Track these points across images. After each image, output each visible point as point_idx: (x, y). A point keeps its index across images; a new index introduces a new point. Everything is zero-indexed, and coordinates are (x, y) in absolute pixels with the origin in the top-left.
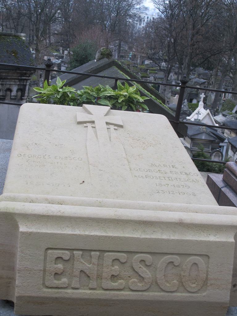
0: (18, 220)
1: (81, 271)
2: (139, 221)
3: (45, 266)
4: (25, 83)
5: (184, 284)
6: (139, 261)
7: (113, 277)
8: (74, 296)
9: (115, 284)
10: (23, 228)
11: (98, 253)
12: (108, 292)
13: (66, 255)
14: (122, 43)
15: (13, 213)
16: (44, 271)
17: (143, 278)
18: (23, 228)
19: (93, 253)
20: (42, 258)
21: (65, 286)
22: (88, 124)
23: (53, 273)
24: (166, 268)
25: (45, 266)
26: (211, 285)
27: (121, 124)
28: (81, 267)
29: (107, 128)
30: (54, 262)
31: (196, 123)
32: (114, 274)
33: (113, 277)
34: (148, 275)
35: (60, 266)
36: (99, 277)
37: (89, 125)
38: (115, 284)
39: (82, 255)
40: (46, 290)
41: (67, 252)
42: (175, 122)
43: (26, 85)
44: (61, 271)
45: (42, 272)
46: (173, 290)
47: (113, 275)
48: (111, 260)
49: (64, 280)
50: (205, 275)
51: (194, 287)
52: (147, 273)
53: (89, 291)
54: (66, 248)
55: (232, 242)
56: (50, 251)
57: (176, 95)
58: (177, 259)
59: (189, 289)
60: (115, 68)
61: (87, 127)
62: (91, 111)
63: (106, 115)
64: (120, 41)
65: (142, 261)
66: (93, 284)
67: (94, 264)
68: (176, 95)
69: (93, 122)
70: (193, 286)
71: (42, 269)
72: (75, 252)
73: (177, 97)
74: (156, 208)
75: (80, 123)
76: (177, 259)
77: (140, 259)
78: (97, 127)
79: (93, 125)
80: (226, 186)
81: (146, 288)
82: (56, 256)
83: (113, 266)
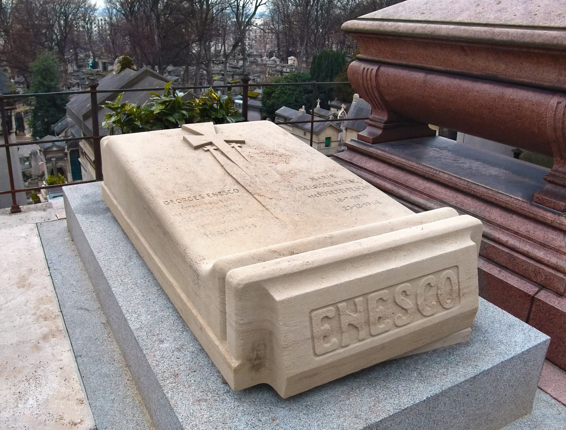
0: (267, 287)
2: (389, 249)
4: (9, 114)
5: (442, 302)
8: (347, 354)
10: (280, 295)
11: (361, 298)
13: (330, 311)
14: (78, 51)
15: (260, 281)
16: (313, 338)
17: (406, 310)
19: (357, 300)
23: (322, 337)
32: (381, 315)
35: (327, 326)
36: (368, 323)
40: (317, 359)
43: (11, 116)
45: (310, 341)
49: (334, 340)
50: (457, 287)
54: (330, 303)
58: (431, 279)
60: (150, 79)
64: (75, 49)
66: (363, 333)
71: (309, 336)
76: (431, 279)
77: (402, 290)
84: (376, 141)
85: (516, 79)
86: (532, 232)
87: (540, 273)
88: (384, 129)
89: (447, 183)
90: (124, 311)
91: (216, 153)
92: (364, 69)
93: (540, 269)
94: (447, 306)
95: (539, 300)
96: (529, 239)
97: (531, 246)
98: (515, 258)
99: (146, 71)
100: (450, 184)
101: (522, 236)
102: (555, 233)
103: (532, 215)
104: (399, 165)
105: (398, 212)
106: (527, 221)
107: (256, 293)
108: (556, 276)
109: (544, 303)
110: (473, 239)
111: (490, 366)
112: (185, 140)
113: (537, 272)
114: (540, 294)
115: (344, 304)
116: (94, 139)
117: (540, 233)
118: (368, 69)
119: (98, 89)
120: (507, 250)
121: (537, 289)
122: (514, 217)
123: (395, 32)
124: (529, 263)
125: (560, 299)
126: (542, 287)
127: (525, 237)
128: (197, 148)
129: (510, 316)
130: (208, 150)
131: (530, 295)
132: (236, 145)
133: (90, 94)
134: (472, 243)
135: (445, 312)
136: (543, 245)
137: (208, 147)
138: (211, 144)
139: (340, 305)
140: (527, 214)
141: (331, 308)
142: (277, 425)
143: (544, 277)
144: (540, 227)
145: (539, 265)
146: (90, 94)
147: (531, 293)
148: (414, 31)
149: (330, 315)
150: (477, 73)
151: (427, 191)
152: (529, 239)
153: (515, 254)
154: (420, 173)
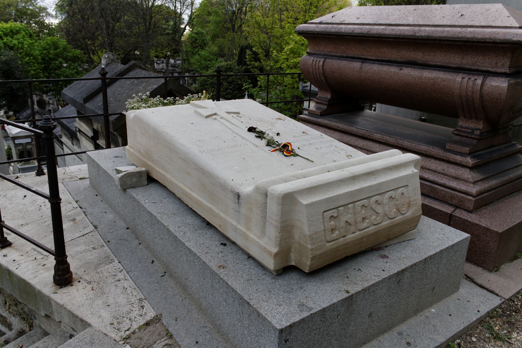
9: (365, 225)
13: (334, 213)
17: (378, 213)
18: (305, 201)
32: (364, 216)
38: (365, 225)
40: (327, 244)
47: (363, 218)
56: (325, 214)
84: (323, 114)
85: (430, 63)
86: (446, 170)
87: (454, 197)
88: (328, 105)
89: (380, 140)
90: (173, 231)
91: (221, 120)
92: (313, 60)
93: (454, 194)
94: (403, 213)
95: (456, 216)
96: (445, 175)
97: (446, 179)
98: (435, 189)
99: (134, 64)
100: (382, 141)
101: (439, 173)
102: (463, 169)
103: (445, 158)
104: (343, 130)
105: (361, 155)
106: (442, 163)
107: (289, 199)
108: (466, 199)
109: (459, 218)
110: (415, 168)
111: (434, 252)
112: (196, 112)
113: (452, 197)
114: (455, 212)
115: (342, 208)
116: (104, 116)
117: (452, 170)
118: (317, 61)
119: (107, 76)
120: (429, 184)
121: (453, 209)
122: (432, 160)
123: (338, 32)
124: (446, 191)
125: (470, 214)
126: (457, 207)
127: (442, 173)
128: (207, 117)
129: (440, 223)
130: (216, 119)
131: (448, 214)
132: (235, 115)
133: (100, 80)
134: (416, 171)
135: (401, 217)
136: (456, 178)
137: (215, 117)
138: (215, 114)
139: (340, 209)
140: (442, 158)
141: (335, 210)
142: (304, 291)
143: (458, 200)
144: (451, 166)
145: (453, 192)
146: (100, 80)
147: (449, 212)
148: (370, 31)
149: (335, 215)
150: (401, 60)
151: (365, 147)
152: (445, 175)
153: (435, 186)
154: (360, 135)
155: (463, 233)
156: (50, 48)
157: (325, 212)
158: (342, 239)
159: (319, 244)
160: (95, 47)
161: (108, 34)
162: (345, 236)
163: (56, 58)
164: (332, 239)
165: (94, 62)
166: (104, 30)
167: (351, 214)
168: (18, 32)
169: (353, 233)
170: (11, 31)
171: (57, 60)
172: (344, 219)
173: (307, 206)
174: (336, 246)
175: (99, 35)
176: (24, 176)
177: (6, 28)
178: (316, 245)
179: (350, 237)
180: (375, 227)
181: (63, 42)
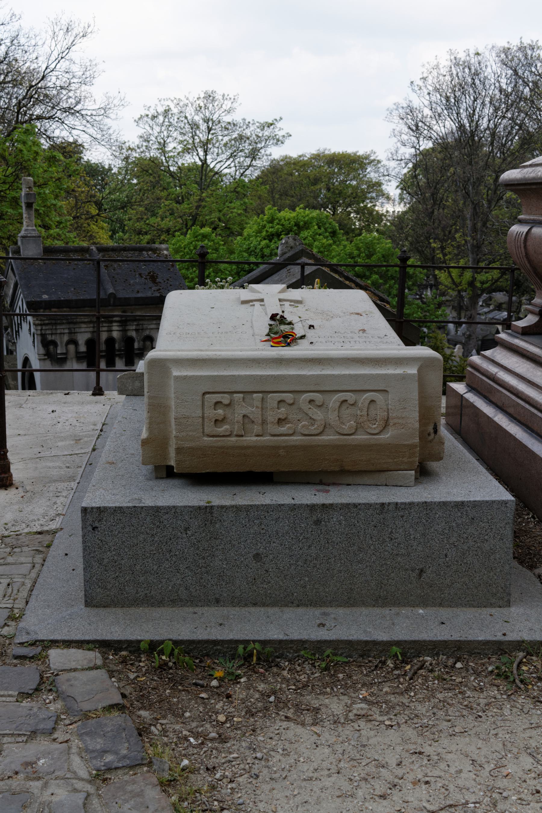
1: (244, 416)
3: (203, 413)
6: (308, 401)
7: (280, 421)
9: (283, 429)
10: (176, 372)
11: (260, 395)
12: (276, 438)
17: (314, 420)
18: (176, 372)
20: (200, 403)
21: (227, 434)
22: (255, 303)
24: (339, 407)
25: (203, 413)
26: (395, 424)
27: (300, 299)
28: (244, 411)
29: (280, 300)
30: (213, 407)
31: (374, 264)
32: (281, 416)
33: (280, 421)
34: (319, 416)
37: (257, 304)
38: (283, 429)
39: (244, 398)
40: (206, 438)
41: (226, 395)
42: (397, 320)
44: (222, 417)
46: (350, 433)
47: (279, 419)
48: (276, 402)
51: (375, 428)
52: (318, 415)
53: (255, 438)
55: (414, 374)
56: (207, 396)
57: (455, 345)
59: (369, 431)
61: (254, 305)
62: (260, 290)
63: (280, 292)
65: (311, 401)
67: (257, 407)
68: (458, 346)
69: (262, 300)
70: (375, 427)
71: (201, 415)
72: (235, 395)
73: (459, 348)
74: (324, 350)
75: (244, 302)
78: (266, 305)
79: (262, 303)
80: (469, 391)
81: (319, 431)
82: (215, 401)
83: (278, 408)
155: (502, 489)
156: (359, 256)
157: (209, 393)
158: (234, 439)
159: (191, 433)
160: (445, 255)
161: (474, 229)
162: (242, 436)
163: (368, 273)
164: (214, 433)
165: (440, 283)
166: (468, 222)
167: (257, 407)
168: (307, 225)
169: (258, 436)
170: (297, 224)
171: (368, 278)
172: (240, 410)
173: (177, 378)
174: (219, 444)
175: (457, 231)
176: (77, 394)
177: (289, 220)
178: (184, 434)
179: (251, 439)
180: (303, 438)
181: (386, 244)
